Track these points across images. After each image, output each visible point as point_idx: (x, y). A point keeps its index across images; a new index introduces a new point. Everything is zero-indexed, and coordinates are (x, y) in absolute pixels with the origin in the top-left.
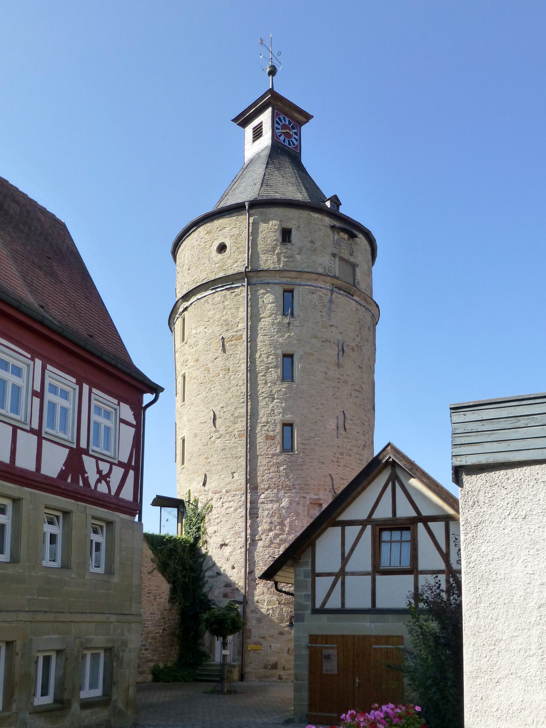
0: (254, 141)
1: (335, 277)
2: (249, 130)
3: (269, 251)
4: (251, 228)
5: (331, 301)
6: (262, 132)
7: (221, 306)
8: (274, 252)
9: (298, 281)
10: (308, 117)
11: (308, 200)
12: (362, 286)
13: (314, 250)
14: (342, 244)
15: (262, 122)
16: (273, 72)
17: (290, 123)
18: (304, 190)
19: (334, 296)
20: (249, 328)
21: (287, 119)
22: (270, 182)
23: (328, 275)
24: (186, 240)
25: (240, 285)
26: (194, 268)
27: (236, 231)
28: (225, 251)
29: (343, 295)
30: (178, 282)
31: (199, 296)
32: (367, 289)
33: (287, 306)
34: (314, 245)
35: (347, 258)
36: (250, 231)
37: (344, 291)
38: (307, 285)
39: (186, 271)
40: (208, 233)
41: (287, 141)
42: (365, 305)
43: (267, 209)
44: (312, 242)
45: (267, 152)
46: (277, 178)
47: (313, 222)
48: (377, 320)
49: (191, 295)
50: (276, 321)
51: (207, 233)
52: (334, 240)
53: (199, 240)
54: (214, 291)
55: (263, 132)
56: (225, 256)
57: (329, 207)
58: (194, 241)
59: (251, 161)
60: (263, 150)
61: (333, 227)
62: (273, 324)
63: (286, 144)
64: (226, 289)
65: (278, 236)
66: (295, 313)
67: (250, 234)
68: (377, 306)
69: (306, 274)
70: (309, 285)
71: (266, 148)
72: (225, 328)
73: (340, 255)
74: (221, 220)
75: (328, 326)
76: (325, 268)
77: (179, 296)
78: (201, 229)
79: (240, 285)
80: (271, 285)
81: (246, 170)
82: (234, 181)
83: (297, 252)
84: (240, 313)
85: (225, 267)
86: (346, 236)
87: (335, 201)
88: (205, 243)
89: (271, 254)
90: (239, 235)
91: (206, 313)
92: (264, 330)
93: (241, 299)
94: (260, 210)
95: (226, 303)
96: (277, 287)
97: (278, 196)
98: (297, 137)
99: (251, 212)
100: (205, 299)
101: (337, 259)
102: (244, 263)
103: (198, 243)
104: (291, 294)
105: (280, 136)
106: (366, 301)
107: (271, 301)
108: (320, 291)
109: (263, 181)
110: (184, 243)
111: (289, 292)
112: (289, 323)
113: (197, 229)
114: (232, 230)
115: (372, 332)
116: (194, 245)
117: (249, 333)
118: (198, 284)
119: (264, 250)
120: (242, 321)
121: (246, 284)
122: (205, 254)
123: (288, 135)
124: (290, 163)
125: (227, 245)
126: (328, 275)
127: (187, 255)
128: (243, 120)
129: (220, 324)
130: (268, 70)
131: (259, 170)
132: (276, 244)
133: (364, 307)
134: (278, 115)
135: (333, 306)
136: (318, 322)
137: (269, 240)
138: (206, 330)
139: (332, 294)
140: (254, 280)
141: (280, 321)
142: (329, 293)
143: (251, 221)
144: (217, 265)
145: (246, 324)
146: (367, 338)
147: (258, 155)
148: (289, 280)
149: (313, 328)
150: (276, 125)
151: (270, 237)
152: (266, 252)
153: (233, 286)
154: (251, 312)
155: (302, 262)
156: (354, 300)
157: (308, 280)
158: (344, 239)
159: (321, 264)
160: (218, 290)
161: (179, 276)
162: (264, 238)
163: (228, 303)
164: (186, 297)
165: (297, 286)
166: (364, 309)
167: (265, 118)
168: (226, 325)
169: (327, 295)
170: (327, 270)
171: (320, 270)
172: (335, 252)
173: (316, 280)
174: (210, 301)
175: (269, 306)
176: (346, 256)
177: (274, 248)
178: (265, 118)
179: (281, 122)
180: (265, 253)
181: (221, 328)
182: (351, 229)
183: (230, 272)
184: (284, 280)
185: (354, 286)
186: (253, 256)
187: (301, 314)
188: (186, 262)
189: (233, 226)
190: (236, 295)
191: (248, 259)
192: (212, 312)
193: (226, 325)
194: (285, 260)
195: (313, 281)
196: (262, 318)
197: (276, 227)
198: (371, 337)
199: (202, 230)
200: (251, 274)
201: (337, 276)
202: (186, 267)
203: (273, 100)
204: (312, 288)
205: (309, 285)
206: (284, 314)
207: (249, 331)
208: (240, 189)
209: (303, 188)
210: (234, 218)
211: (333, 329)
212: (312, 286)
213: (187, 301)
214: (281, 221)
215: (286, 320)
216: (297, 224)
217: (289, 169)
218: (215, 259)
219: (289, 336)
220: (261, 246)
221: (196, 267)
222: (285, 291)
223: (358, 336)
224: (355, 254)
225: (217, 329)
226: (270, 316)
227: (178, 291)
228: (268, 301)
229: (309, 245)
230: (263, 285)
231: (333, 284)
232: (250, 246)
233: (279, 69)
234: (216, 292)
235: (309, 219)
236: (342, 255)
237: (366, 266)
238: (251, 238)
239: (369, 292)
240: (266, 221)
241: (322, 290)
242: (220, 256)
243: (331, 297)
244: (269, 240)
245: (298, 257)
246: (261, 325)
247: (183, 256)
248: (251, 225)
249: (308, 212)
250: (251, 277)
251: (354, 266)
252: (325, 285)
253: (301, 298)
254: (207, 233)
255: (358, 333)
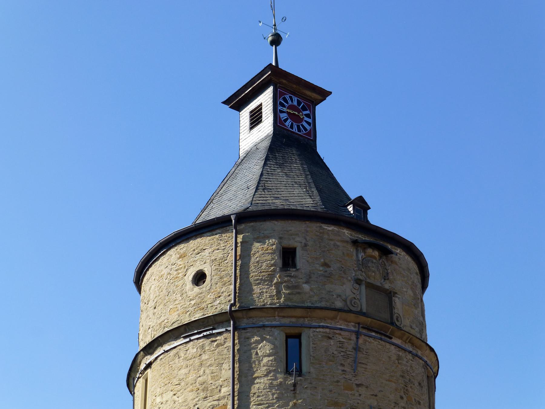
0: (251, 128)
1: (361, 313)
2: (245, 114)
3: (265, 281)
4: (239, 249)
5: (357, 349)
6: (261, 117)
7: (197, 361)
8: (272, 282)
9: (306, 321)
10: (324, 94)
11: (320, 208)
12: (406, 323)
13: (329, 277)
14: (370, 264)
15: (261, 105)
16: (276, 41)
17: (299, 103)
18: (315, 192)
19: (361, 341)
20: (236, 394)
21: (295, 99)
22: (268, 185)
23: (350, 311)
24: (153, 266)
25: (224, 330)
26: (161, 306)
27: (219, 255)
28: (204, 282)
29: (375, 338)
30: (141, 324)
31: (166, 347)
32: (414, 326)
33: (291, 360)
34: (328, 269)
35: (379, 284)
36: (239, 253)
37: (376, 332)
38: (319, 327)
39: (151, 311)
40: (182, 257)
41: (295, 127)
42: (411, 349)
43: (261, 223)
44: (325, 265)
45: (267, 143)
46: (279, 178)
47: (326, 236)
48: (435, 370)
49: (156, 345)
50: (275, 383)
51: (180, 258)
52: (359, 260)
53: (169, 267)
54: (188, 340)
55: (263, 116)
56: (204, 289)
57: (352, 212)
58: (163, 267)
59: (248, 154)
60: (262, 140)
61: (355, 243)
62: (271, 386)
63: (295, 130)
64: (204, 337)
65: (277, 259)
66: (304, 369)
67: (238, 258)
68: (432, 350)
69: (318, 311)
70: (323, 327)
71: (266, 137)
72: (202, 395)
73: (368, 280)
74: (199, 240)
75: (355, 386)
76: (345, 301)
77: (143, 345)
78: (172, 252)
79: (224, 330)
80: (268, 329)
81: (240, 167)
82: (224, 182)
83: (304, 280)
84: (223, 371)
85: (204, 305)
86: (376, 253)
87: (361, 205)
88: (176, 270)
89: (267, 285)
90: (224, 259)
91: (175, 372)
92: (258, 396)
93: (226, 351)
94: (252, 224)
95: (204, 357)
96: (276, 332)
97: (279, 204)
98: (310, 121)
99: (242, 227)
100: (174, 351)
101: (363, 287)
102: (229, 298)
103: (168, 270)
104: (297, 340)
105: (286, 120)
106: (413, 344)
107: (268, 352)
108: (340, 334)
109: (259, 183)
110: (150, 269)
111: (293, 338)
112: (295, 385)
113: (167, 251)
114: (213, 253)
115: (425, 389)
116: (163, 273)
117: (236, 402)
118: (167, 330)
119: (258, 280)
120: (226, 383)
121: (231, 328)
122: (177, 286)
123: (296, 119)
124: (299, 155)
125: (207, 273)
126: (350, 311)
127: (153, 287)
128: (237, 102)
129: (195, 389)
130: (270, 39)
131: (254, 168)
132: (274, 271)
133: (410, 352)
134: (281, 94)
135: (360, 355)
136: (338, 381)
137: (264, 264)
138: (175, 397)
139: (357, 338)
140: (244, 323)
141: (281, 383)
142: (354, 337)
143: (239, 240)
144: (193, 302)
145: (231, 388)
146: (417, 399)
147: (256, 148)
148: (294, 320)
149: (331, 391)
150: (280, 108)
151: (266, 260)
152: (261, 282)
153: (214, 332)
154: (240, 370)
155: (312, 293)
156: (394, 344)
157: (324, 319)
158: (375, 258)
159: (340, 296)
160: (192, 338)
161: (144, 316)
162: (258, 262)
163: (207, 357)
164: (149, 348)
165: (306, 330)
166: (410, 357)
167: (266, 99)
168: (203, 390)
169: (350, 339)
170: (348, 303)
171: (339, 304)
172: (361, 277)
173: (333, 319)
174: (182, 354)
175: (265, 360)
176: (378, 281)
177: (271, 276)
178: (266, 99)
179: (287, 103)
180: (259, 284)
181: (196, 395)
182: (385, 243)
183: (210, 313)
184: (286, 321)
185: (392, 323)
186: (243, 287)
187: (312, 370)
188: (152, 296)
189: (214, 247)
190: (218, 346)
191: (235, 293)
192: (183, 371)
193: (203, 390)
194: (287, 292)
195: (329, 321)
196: (256, 378)
197: (274, 247)
198: (426, 397)
199: (173, 254)
200: (239, 314)
201: (364, 311)
202: (152, 304)
203: (275, 77)
204: (328, 330)
205: (323, 327)
206: (288, 372)
207: (236, 398)
208: (229, 195)
209: (314, 189)
210: (217, 236)
211: (362, 390)
212: (327, 327)
213: (151, 354)
214: (281, 238)
215: (291, 381)
216: (304, 241)
217: (297, 166)
218: (190, 293)
219: (295, 404)
220: (254, 274)
221: (165, 305)
222: (288, 337)
223: (402, 398)
224: (391, 277)
225: (191, 396)
226: (266, 375)
227: (141, 337)
228: (264, 351)
229: (321, 269)
230: (255, 330)
231: (359, 324)
232: (238, 274)
233: (285, 37)
234: (191, 341)
235: (321, 233)
236: (371, 281)
237: (410, 292)
238: (239, 263)
239: (417, 329)
240: (261, 239)
241: (343, 333)
242: (197, 289)
243: (357, 341)
244: (264, 264)
245: (306, 287)
246: (255, 389)
247: (148, 288)
248: (239, 245)
249: (318, 224)
250: (240, 319)
251: (390, 295)
252: (347, 325)
253: (311, 345)
254: (180, 258)
255: (402, 394)
